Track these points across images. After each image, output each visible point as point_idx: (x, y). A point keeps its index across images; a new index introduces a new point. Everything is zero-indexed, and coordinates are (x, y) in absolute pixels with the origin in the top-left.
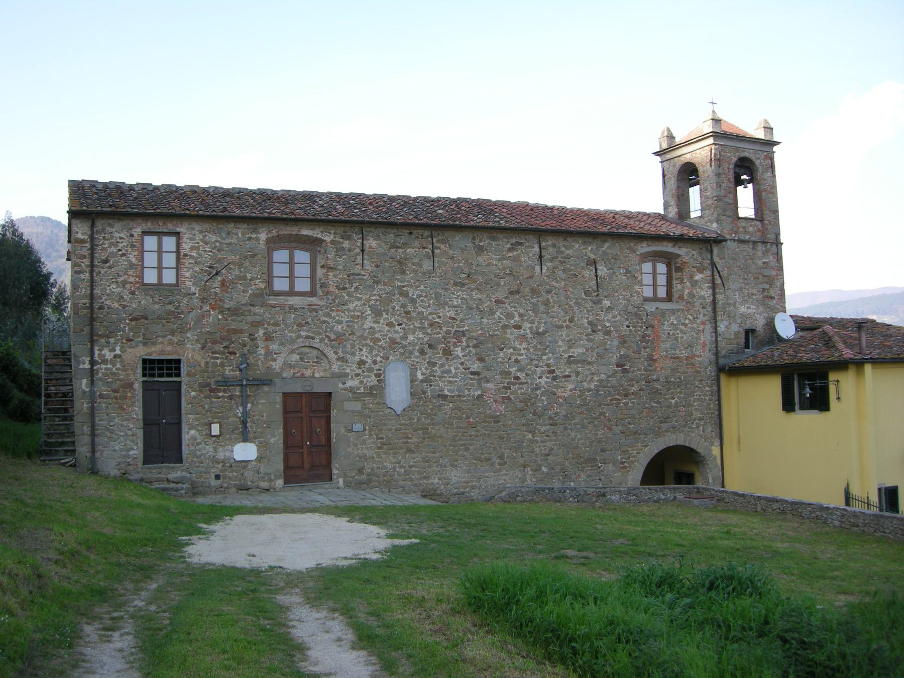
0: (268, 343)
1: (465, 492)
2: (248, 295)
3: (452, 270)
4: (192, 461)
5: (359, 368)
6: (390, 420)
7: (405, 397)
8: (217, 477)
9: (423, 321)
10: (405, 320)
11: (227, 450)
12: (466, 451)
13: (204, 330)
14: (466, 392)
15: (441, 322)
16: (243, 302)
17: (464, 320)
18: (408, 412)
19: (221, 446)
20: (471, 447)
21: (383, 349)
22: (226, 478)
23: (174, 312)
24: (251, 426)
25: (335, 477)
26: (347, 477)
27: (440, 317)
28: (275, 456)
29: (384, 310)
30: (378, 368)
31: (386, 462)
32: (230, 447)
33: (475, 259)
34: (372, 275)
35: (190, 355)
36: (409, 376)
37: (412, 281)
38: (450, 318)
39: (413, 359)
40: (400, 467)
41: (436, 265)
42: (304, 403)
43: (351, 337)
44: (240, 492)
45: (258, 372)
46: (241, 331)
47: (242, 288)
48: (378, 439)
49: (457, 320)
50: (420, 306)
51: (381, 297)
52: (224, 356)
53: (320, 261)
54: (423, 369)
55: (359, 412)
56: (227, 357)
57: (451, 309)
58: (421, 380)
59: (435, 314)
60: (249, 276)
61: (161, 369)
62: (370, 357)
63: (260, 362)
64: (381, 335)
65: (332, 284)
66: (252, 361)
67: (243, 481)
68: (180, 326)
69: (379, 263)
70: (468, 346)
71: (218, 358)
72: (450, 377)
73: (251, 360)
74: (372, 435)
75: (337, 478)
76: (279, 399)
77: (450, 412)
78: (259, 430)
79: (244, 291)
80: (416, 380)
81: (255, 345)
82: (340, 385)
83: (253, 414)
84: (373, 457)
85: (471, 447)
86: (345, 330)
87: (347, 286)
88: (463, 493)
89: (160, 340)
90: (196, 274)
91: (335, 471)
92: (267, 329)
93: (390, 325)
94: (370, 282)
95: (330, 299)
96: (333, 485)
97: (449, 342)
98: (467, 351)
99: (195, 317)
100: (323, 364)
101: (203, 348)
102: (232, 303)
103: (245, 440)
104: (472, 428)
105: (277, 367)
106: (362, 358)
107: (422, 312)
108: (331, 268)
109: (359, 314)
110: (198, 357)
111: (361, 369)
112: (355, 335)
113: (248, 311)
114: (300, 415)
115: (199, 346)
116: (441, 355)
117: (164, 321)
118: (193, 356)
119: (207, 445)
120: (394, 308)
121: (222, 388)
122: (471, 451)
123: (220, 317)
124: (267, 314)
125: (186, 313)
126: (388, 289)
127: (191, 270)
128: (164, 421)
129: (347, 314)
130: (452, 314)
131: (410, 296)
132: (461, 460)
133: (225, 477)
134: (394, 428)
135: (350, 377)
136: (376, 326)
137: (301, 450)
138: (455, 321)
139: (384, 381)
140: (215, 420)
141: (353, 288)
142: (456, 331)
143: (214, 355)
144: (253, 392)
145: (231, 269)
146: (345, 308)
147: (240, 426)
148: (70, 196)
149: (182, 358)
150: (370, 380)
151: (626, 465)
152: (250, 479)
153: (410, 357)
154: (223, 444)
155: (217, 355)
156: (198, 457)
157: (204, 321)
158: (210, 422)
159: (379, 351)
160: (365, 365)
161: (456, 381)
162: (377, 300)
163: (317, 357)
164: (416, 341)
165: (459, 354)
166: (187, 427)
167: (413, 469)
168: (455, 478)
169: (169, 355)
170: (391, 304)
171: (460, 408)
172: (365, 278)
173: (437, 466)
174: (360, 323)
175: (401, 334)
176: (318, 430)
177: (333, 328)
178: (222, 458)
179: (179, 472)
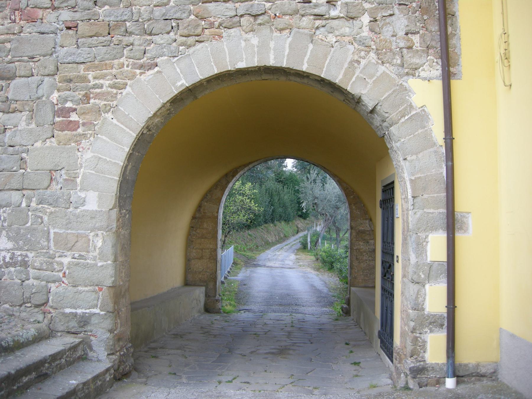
148: (432, 315)
151: (74, 117)
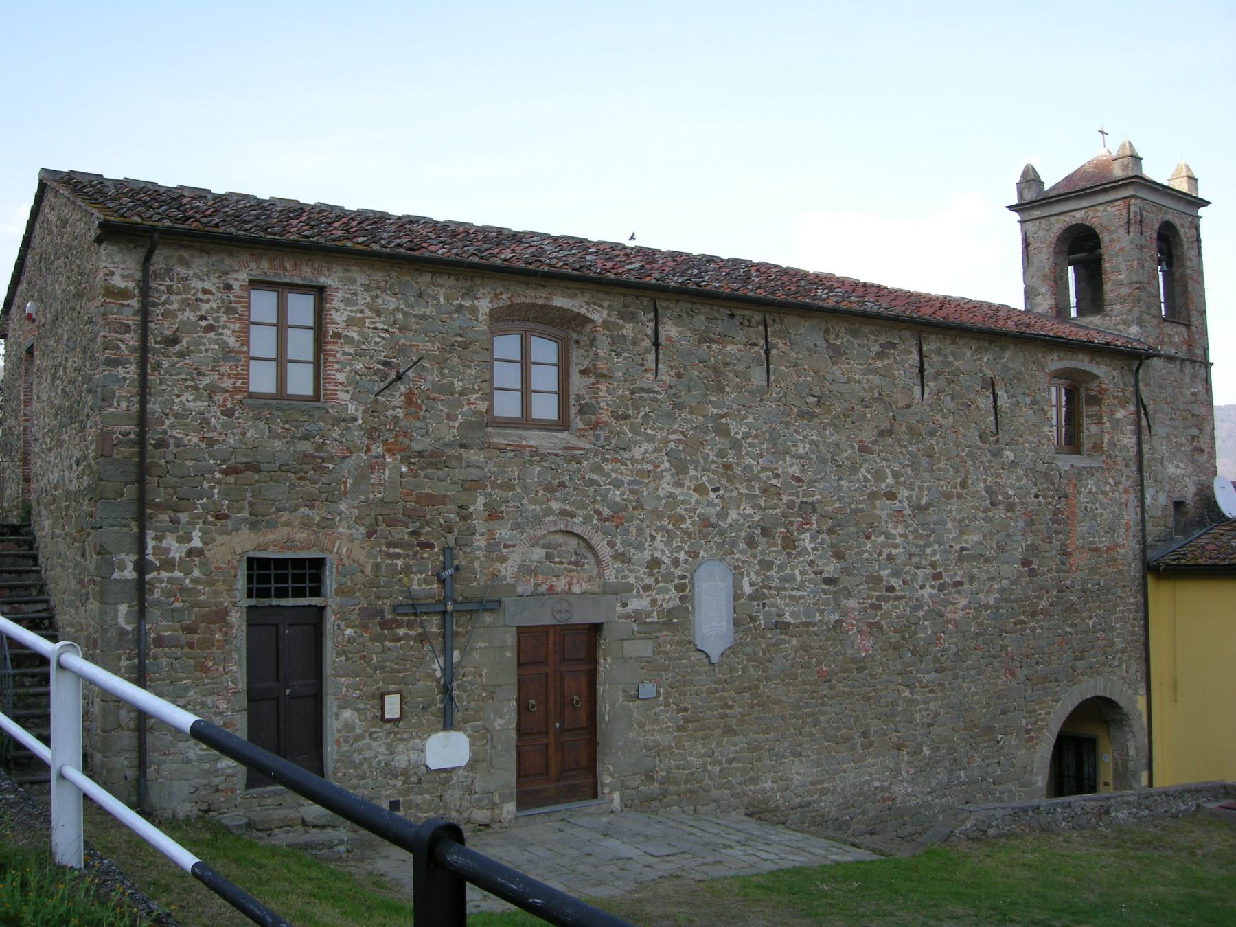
2: (457, 424)
4: (345, 775)
5: (651, 574)
6: (700, 674)
11: (413, 748)
12: (815, 726)
13: (372, 497)
15: (779, 485)
16: (447, 440)
17: (815, 481)
20: (822, 719)
21: (690, 536)
29: (691, 462)
30: (680, 573)
31: (690, 755)
34: (671, 391)
35: (345, 550)
37: (735, 407)
40: (713, 764)
43: (636, 513)
45: (475, 584)
46: (443, 500)
51: (686, 436)
55: (650, 661)
56: (416, 553)
57: (794, 460)
58: (749, 595)
59: (771, 470)
60: (458, 385)
61: (281, 579)
62: (667, 552)
70: (819, 532)
71: (398, 556)
72: (792, 590)
75: (611, 793)
76: (511, 639)
78: (473, 704)
81: (468, 530)
82: (619, 609)
85: (822, 719)
88: (809, 804)
89: (285, 516)
90: (358, 377)
93: (701, 489)
94: (667, 406)
95: (602, 437)
97: (791, 523)
98: (819, 540)
100: (586, 566)
101: (370, 535)
105: (509, 574)
106: (656, 555)
107: (750, 466)
108: (603, 376)
109: (651, 468)
110: (359, 554)
115: (363, 530)
116: (780, 548)
117: (293, 476)
118: (349, 552)
119: (374, 739)
120: (706, 458)
121: (405, 618)
123: (404, 469)
126: (697, 420)
127: (348, 369)
128: (288, 692)
129: (631, 467)
130: (795, 470)
134: (704, 688)
136: (677, 491)
140: (392, 687)
142: (802, 502)
143: (392, 551)
145: (424, 369)
146: (627, 455)
149: (329, 557)
150: (667, 597)
153: (733, 553)
154: (406, 736)
155: (398, 550)
156: (356, 767)
162: (679, 441)
163: (576, 553)
164: (741, 521)
165: (807, 545)
166: (335, 705)
167: (734, 765)
173: (770, 758)
174: (652, 485)
178: (404, 765)
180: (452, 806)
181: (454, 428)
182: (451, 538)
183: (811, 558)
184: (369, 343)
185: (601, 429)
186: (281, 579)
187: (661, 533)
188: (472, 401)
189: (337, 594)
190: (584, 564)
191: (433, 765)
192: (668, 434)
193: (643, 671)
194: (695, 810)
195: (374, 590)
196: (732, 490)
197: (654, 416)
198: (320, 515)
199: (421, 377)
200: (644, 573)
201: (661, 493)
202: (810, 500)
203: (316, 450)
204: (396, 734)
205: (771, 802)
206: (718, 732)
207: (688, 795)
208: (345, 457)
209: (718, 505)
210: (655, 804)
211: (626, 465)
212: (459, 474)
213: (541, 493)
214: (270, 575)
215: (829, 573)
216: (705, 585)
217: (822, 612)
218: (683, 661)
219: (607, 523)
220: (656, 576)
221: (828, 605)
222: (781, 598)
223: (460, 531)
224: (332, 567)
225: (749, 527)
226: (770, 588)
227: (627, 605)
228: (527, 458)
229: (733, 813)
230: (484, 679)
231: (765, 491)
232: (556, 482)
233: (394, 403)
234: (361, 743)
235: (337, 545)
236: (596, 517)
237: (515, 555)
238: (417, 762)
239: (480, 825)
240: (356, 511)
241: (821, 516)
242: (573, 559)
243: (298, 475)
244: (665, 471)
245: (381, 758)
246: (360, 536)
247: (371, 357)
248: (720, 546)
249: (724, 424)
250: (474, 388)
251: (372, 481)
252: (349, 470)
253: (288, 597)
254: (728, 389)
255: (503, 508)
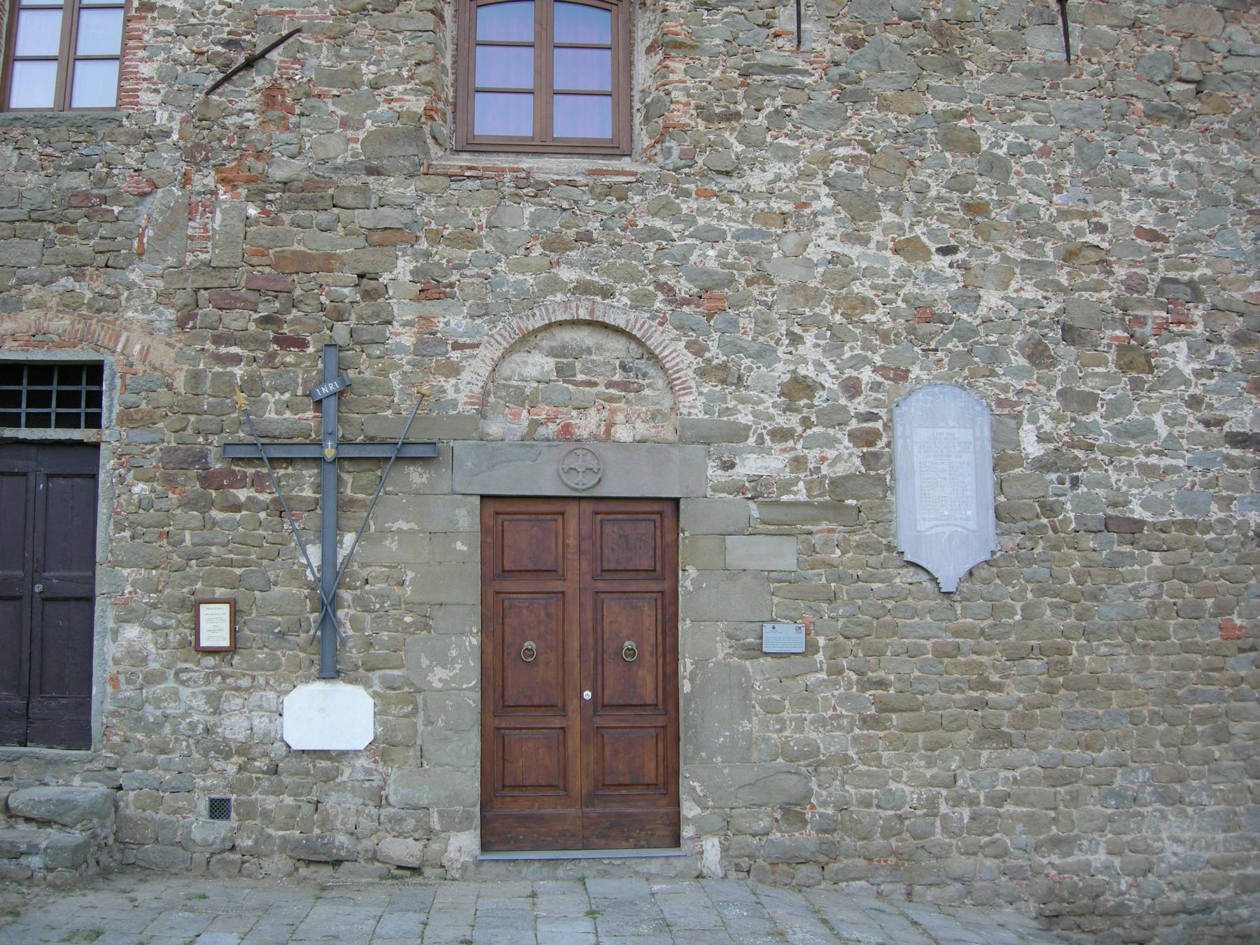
0: (431, 307)
1: (1219, 903)
2: (361, 135)
3: (1135, 67)
4: (126, 740)
5: (789, 409)
6: (915, 613)
7: (972, 525)
8: (219, 809)
9: (1039, 240)
10: (967, 235)
11: (260, 707)
12: (1218, 742)
13: (189, 258)
14: (1215, 512)
15: (1105, 245)
16: (339, 161)
17: (1195, 241)
18: (986, 582)
19: (238, 689)
20: (1236, 728)
21: (885, 337)
22: (249, 815)
23: (87, 196)
24: (353, 620)
25: (687, 832)
26: (739, 832)
27: (1101, 228)
28: (447, 740)
29: (886, 198)
30: (863, 409)
31: (897, 778)
32: (272, 695)
33: (1217, 31)
34: (835, 72)
35: (138, 347)
36: (988, 444)
37: (990, 97)
38: (1140, 232)
39: (1004, 380)
40: (956, 801)
41: (1077, 45)
42: (572, 541)
43: (755, 291)
44: (303, 871)
45: (389, 413)
46: (327, 263)
47: (340, 112)
48: (865, 685)
49: (1166, 241)
50: (1023, 184)
51: (872, 151)
52: (260, 354)
53: (645, 31)
54: (1043, 417)
55: (787, 579)
56: (272, 356)
57: (1140, 198)
58: (1038, 460)
59: (1083, 215)
60: (368, 71)
61: (38, 399)
62: (831, 367)
63: (395, 378)
64: (874, 287)
65: (684, 99)
66: (367, 374)
67: (317, 831)
68: (108, 245)
69: (860, 34)
70: (1211, 340)
71: (236, 360)
72: (1148, 453)
73: (364, 369)
74: (840, 672)
75: (697, 837)
76: (467, 517)
77: (1152, 588)
78: (385, 635)
79: (344, 123)
80: (1017, 461)
81: (376, 314)
82: (714, 473)
83: (364, 573)
84: (846, 759)
85: (1236, 728)
86: (731, 266)
87: (740, 108)
88: (1207, 908)
89: (33, 292)
90: (180, 68)
91: (689, 810)
92: (428, 255)
93: (908, 249)
94: (826, 96)
95: (676, 152)
96: (680, 864)
97: (1141, 321)
98: (1212, 356)
99: (161, 212)
100: (647, 392)
101: (182, 324)
102: (298, 163)
103: (331, 672)
104: (1242, 650)
105: (462, 398)
106: (802, 371)
107: (1031, 208)
108: (678, 45)
109: (788, 207)
110: (163, 355)
111: (797, 411)
112: (772, 284)
113: (356, 190)
114: (557, 585)
115: (170, 314)
116: (1113, 368)
117: (51, 228)
118: (145, 352)
119: (183, 683)
120: (921, 192)
121: (250, 471)
122: (1237, 741)
123: (252, 211)
124: (430, 204)
125: (131, 200)
126: (897, 121)
127: (162, 56)
128: (38, 588)
129: (742, 205)
130: (1146, 216)
131: (985, 148)
132: (1200, 775)
133: (249, 811)
134: (929, 644)
135: (752, 441)
136: (854, 251)
137: (557, 722)
138: (1159, 245)
139: (891, 461)
140: (220, 592)
141: (761, 116)
142: (1165, 280)
143: (223, 350)
144: (363, 489)
145: (303, 48)
146: (732, 184)
147: (313, 616)
149: (108, 359)
150: (831, 454)
152: (344, 823)
153: (993, 374)
154: (245, 682)
155: (234, 350)
156: (149, 730)
157: (194, 228)
158: (199, 596)
159: (867, 346)
160: (811, 397)
161: (1176, 469)
162: (856, 159)
163: (623, 367)
164: (1013, 312)
165: (1180, 364)
166: (111, 614)
167: (1009, 807)
168: (1175, 847)
169: (60, 346)
170: (910, 172)
171: (1189, 570)
172: (807, 80)
173: (1102, 801)
174: (791, 240)
175: (953, 287)
176: (628, 644)
177: (685, 258)
178: (241, 737)
179: (77, 781)
180: (338, 824)
181: (356, 140)
182: (341, 332)
183: (1192, 391)
184: (204, 14)
185: (672, 138)
186: (38, 399)
187: (814, 331)
188: (396, 95)
189: (121, 423)
190: (641, 388)
191: (298, 742)
192: (828, 147)
193: (776, 600)
194: (909, 894)
195: (192, 418)
196: (989, 253)
197: (795, 114)
198: (92, 290)
199: (296, 60)
200: (775, 405)
201: (812, 253)
202: (1186, 276)
203: (95, 185)
204: (225, 677)
205: (1107, 896)
206: (965, 736)
207: (892, 860)
208: (144, 195)
209: (953, 279)
210: (811, 871)
211: (731, 203)
212: (363, 218)
213: (537, 251)
214: (79, 393)
215: (1242, 423)
216: (922, 434)
217: (1226, 502)
218: (875, 586)
219: (686, 309)
220: (805, 412)
221: (1244, 488)
222: (1116, 469)
223: (360, 317)
224: (113, 377)
225: (1032, 324)
226: (1090, 448)
227: (732, 466)
228: (507, 191)
229: (1009, 909)
230: (409, 589)
231: (1070, 256)
232: (571, 233)
233: (242, 104)
234: (158, 689)
235: (123, 339)
236: (661, 296)
237: (476, 363)
238: (267, 734)
239: (400, 867)
240: (160, 283)
241: (1214, 308)
242: (616, 378)
243: (59, 225)
244: (824, 213)
245: (196, 718)
246: (165, 325)
247: (205, 36)
248: (959, 360)
249: (963, 130)
250: (399, 74)
251: (190, 232)
252: (149, 217)
253: (49, 426)
254: (970, 66)
255: (453, 278)
